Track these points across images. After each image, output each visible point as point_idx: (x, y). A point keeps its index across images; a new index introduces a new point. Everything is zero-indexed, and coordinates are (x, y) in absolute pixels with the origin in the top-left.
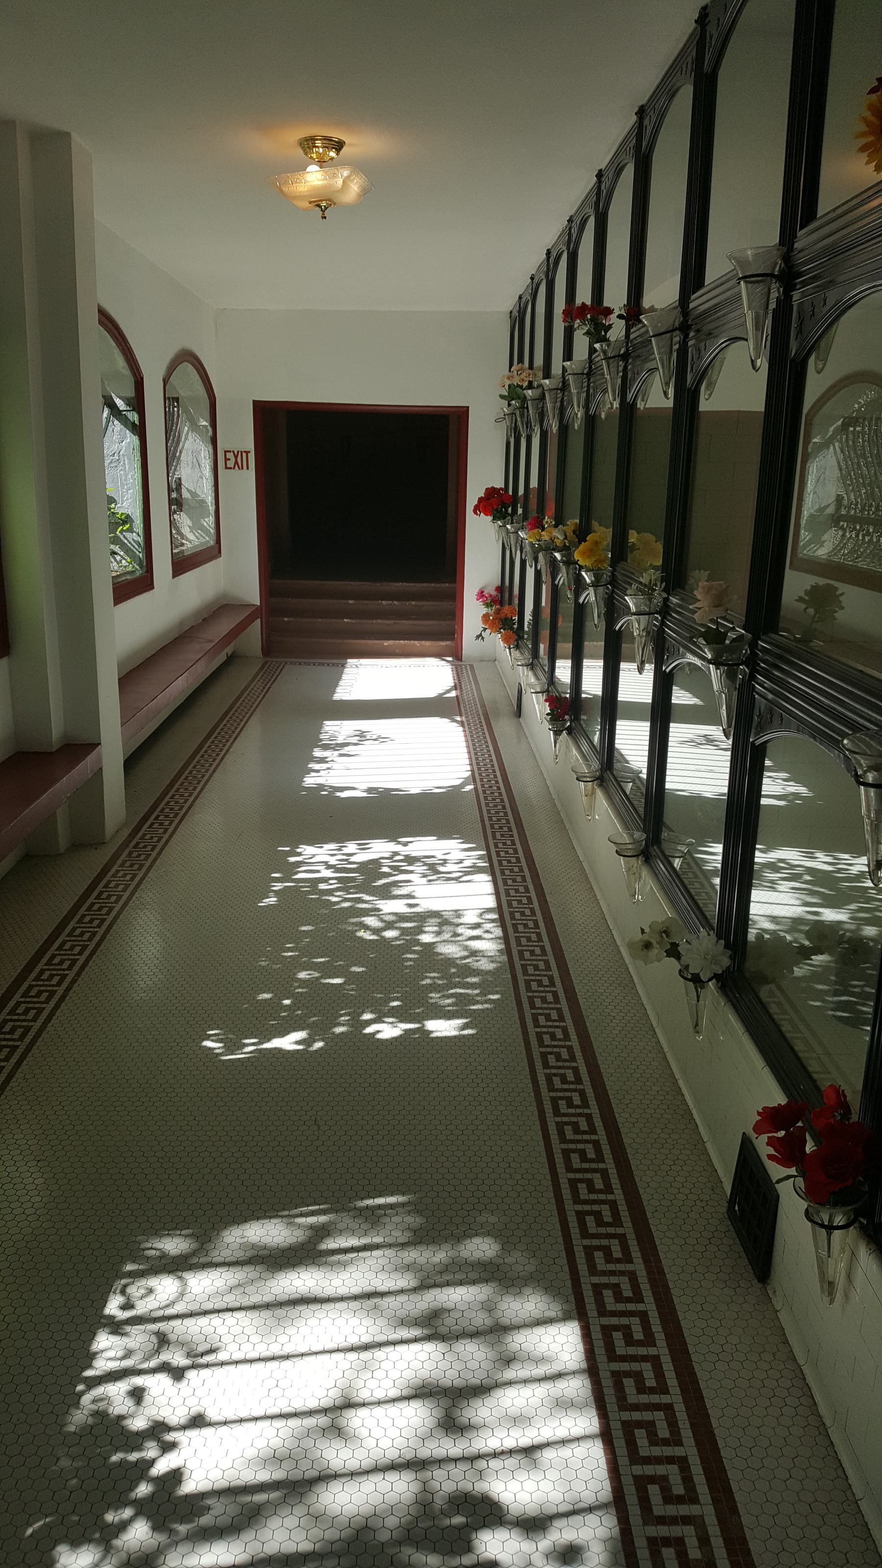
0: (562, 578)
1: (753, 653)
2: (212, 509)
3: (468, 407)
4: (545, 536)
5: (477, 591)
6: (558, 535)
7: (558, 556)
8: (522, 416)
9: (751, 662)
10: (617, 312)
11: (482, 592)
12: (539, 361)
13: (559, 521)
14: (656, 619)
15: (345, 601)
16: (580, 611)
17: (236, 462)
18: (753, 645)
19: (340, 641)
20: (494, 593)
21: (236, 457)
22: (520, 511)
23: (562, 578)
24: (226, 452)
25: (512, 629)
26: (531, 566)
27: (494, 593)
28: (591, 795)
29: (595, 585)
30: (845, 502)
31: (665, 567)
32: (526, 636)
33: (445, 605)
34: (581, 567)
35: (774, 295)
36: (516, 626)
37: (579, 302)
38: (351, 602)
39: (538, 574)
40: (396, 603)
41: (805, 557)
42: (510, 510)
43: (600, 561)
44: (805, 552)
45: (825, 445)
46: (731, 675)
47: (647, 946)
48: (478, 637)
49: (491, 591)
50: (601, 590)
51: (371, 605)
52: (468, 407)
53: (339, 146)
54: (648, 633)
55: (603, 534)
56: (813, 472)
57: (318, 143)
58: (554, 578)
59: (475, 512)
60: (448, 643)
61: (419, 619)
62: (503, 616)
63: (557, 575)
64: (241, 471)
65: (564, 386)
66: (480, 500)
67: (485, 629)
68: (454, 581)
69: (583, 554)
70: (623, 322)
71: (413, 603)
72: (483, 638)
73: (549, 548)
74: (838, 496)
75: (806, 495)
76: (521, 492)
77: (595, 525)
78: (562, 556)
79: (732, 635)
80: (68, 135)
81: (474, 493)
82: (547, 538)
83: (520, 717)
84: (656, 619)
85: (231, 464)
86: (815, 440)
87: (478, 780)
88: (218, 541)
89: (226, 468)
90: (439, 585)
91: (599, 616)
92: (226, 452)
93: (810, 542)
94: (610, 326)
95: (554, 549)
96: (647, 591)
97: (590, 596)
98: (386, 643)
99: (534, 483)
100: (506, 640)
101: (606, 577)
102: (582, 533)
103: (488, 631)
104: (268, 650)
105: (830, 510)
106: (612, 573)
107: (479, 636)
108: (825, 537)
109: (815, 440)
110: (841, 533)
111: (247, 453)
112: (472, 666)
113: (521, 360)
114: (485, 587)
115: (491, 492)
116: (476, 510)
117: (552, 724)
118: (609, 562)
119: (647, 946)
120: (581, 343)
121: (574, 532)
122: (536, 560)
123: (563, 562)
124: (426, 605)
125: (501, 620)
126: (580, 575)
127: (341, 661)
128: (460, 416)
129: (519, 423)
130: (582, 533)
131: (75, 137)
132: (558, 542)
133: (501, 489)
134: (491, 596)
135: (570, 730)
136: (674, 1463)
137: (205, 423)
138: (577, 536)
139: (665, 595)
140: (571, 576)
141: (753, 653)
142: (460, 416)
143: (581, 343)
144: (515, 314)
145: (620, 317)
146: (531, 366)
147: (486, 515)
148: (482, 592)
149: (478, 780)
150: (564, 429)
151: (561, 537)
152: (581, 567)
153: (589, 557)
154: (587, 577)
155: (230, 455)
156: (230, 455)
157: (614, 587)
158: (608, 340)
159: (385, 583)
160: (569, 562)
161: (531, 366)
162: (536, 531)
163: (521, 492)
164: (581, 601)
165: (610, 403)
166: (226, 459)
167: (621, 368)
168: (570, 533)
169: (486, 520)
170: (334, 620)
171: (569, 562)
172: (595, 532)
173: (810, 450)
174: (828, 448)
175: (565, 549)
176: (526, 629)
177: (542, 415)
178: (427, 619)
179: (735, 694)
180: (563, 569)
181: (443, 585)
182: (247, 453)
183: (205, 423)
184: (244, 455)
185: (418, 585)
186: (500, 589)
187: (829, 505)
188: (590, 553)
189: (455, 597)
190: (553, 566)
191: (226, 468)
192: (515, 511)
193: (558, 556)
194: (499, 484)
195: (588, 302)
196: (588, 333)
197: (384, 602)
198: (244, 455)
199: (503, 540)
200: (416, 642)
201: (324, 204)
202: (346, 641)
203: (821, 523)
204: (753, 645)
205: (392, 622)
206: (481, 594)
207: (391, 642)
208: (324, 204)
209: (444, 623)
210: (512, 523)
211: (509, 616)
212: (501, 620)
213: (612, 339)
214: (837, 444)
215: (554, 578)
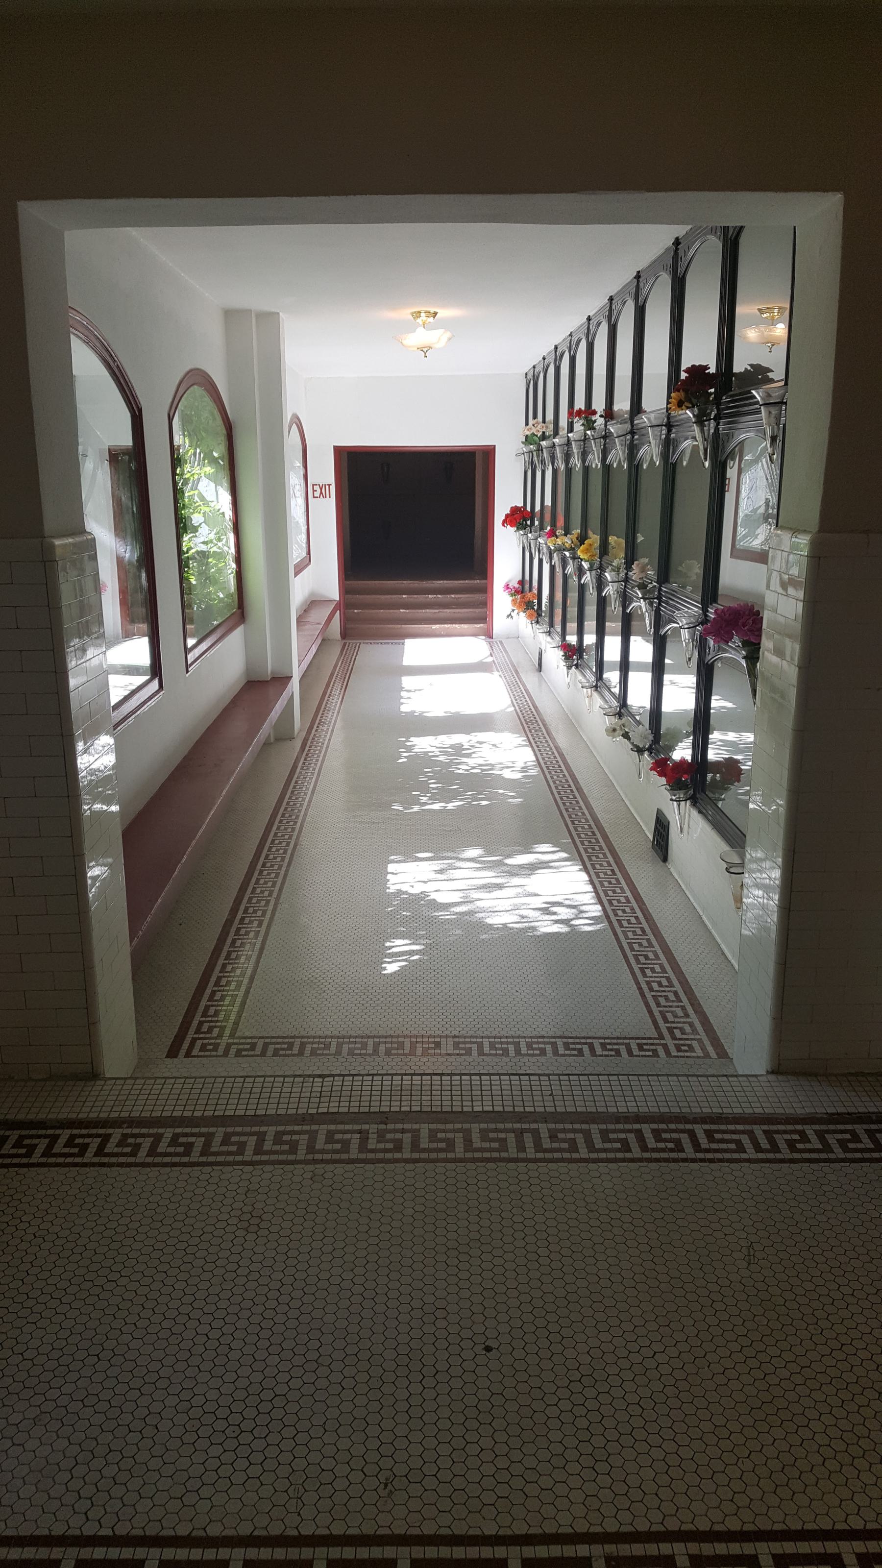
0: (570, 569)
1: (660, 594)
2: (304, 529)
3: (495, 446)
4: (559, 542)
5: (503, 584)
6: (567, 541)
7: (567, 554)
8: (538, 456)
9: (659, 598)
10: (599, 414)
11: (508, 585)
12: (550, 416)
13: (567, 532)
14: (622, 585)
15: (400, 596)
16: (582, 588)
17: (321, 493)
18: (660, 590)
19: (399, 626)
20: (517, 586)
21: (321, 489)
22: (537, 523)
23: (570, 569)
24: (313, 485)
25: (534, 609)
26: (547, 563)
27: (517, 586)
28: (590, 697)
29: (590, 569)
30: (771, 504)
31: (626, 558)
32: (543, 614)
33: (478, 597)
34: (582, 560)
35: (664, 432)
36: (536, 608)
37: (576, 408)
38: (404, 596)
39: (552, 568)
40: (439, 596)
41: (741, 548)
42: (529, 522)
43: (593, 556)
44: (741, 544)
45: (756, 461)
46: (651, 604)
47: (614, 730)
48: (508, 616)
49: (515, 584)
50: (594, 572)
51: (420, 598)
52: (495, 446)
53: (436, 314)
54: (618, 592)
55: (594, 539)
56: (746, 483)
57: (423, 315)
58: (564, 569)
59: (503, 525)
60: (482, 625)
61: (457, 608)
62: (527, 600)
63: (566, 567)
64: (325, 499)
65: (568, 443)
66: (507, 516)
67: (513, 610)
68: (486, 578)
69: (582, 551)
70: (603, 419)
71: (453, 596)
72: (512, 617)
73: (560, 549)
74: (767, 499)
75: (741, 500)
76: (538, 508)
77: (590, 533)
78: (570, 554)
79: (650, 586)
80: (278, 313)
81: (501, 511)
82: (560, 543)
83: (541, 671)
84: (622, 585)
85: (317, 494)
86: (747, 458)
87: (515, 704)
88: (309, 553)
89: (314, 497)
90: (472, 581)
91: (593, 588)
92: (313, 485)
93: (745, 536)
94: (595, 421)
95: (564, 550)
96: (617, 570)
97: (587, 578)
98: (434, 627)
99: (548, 502)
100: (530, 617)
101: (596, 566)
102: (582, 539)
103: (516, 611)
104: (344, 635)
105: (762, 510)
106: (600, 562)
107: (510, 616)
108: (758, 531)
109: (747, 458)
110: (769, 527)
111: (329, 485)
112: (501, 642)
113: (535, 416)
114: (510, 581)
115: (515, 510)
116: (504, 523)
117: (566, 662)
118: (598, 556)
119: (614, 730)
120: (578, 426)
121: (577, 538)
122: (551, 558)
123: (571, 558)
124: (463, 597)
125: (525, 602)
126: (581, 565)
127: (402, 641)
128: (488, 453)
129: (535, 458)
130: (582, 539)
131: (281, 314)
132: (567, 545)
133: (522, 507)
134: (514, 588)
135: (577, 666)
136: (651, 1149)
137: (299, 465)
138: (579, 541)
139: (626, 571)
140: (575, 566)
141: (660, 594)
142: (488, 453)
143: (578, 426)
144: (530, 376)
145: (601, 416)
146: (544, 421)
147: (511, 526)
148: (508, 585)
149: (515, 704)
150: (569, 471)
151: (570, 542)
152: (582, 560)
153: (586, 553)
154: (586, 565)
155: (316, 488)
156: (316, 488)
157: (601, 570)
158: (595, 429)
159: (430, 582)
160: (574, 558)
161: (544, 421)
162: (553, 538)
163: (538, 508)
164: (582, 582)
165: (595, 461)
166: (314, 491)
167: (602, 444)
168: (575, 540)
169: (511, 530)
170: (392, 611)
171: (574, 558)
172: (590, 538)
173: (743, 466)
174: (758, 463)
175: (572, 549)
176: (544, 609)
177: (553, 459)
178: (465, 608)
179: (653, 613)
180: (571, 561)
181: (476, 582)
182: (329, 485)
183: (299, 465)
184: (327, 487)
185: (455, 582)
186: (522, 582)
187: (760, 507)
188: (587, 551)
189: (486, 590)
190: (564, 562)
191: (314, 497)
192: (532, 523)
193: (567, 554)
194: (520, 504)
195: (583, 408)
196: (583, 425)
197: (430, 596)
198: (327, 487)
199: (523, 543)
200: (457, 626)
201: (425, 350)
202: (403, 626)
203: (753, 521)
204: (660, 590)
205: (437, 611)
206: (507, 587)
207: (437, 626)
208: (425, 350)
209: (477, 611)
210: (531, 532)
211: (531, 599)
212: (525, 602)
213: (597, 428)
214: (764, 460)
215: (564, 569)
